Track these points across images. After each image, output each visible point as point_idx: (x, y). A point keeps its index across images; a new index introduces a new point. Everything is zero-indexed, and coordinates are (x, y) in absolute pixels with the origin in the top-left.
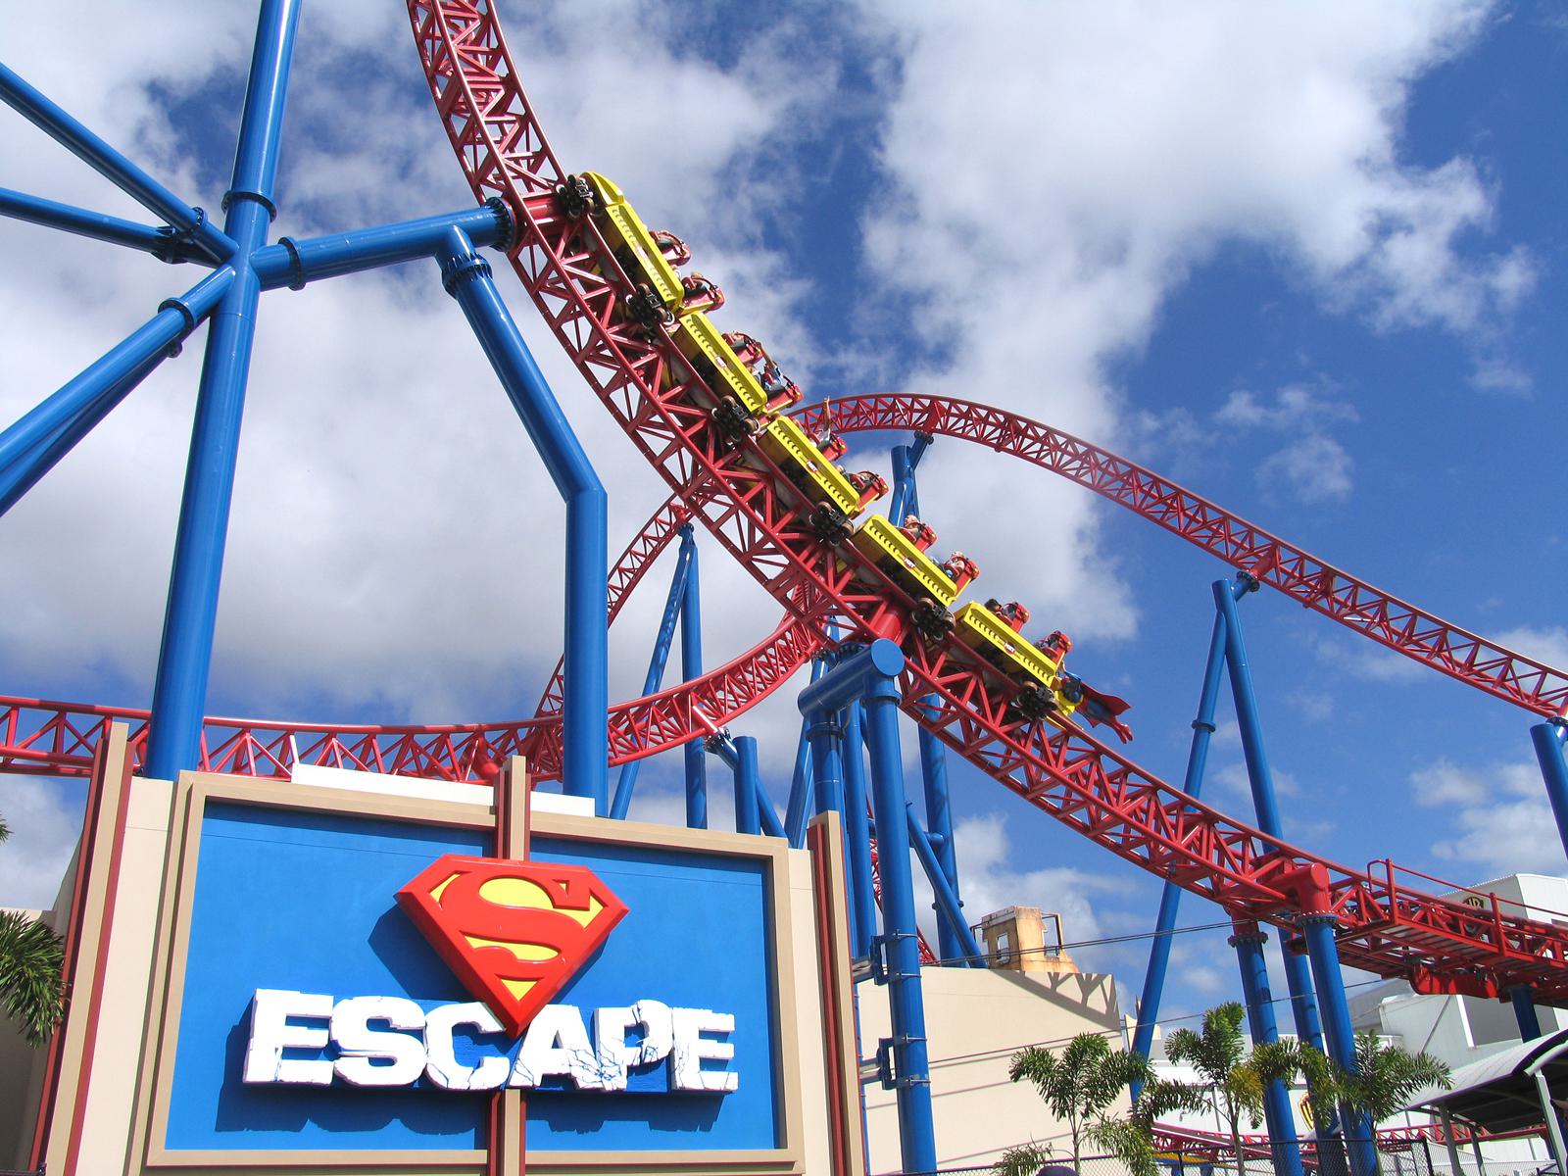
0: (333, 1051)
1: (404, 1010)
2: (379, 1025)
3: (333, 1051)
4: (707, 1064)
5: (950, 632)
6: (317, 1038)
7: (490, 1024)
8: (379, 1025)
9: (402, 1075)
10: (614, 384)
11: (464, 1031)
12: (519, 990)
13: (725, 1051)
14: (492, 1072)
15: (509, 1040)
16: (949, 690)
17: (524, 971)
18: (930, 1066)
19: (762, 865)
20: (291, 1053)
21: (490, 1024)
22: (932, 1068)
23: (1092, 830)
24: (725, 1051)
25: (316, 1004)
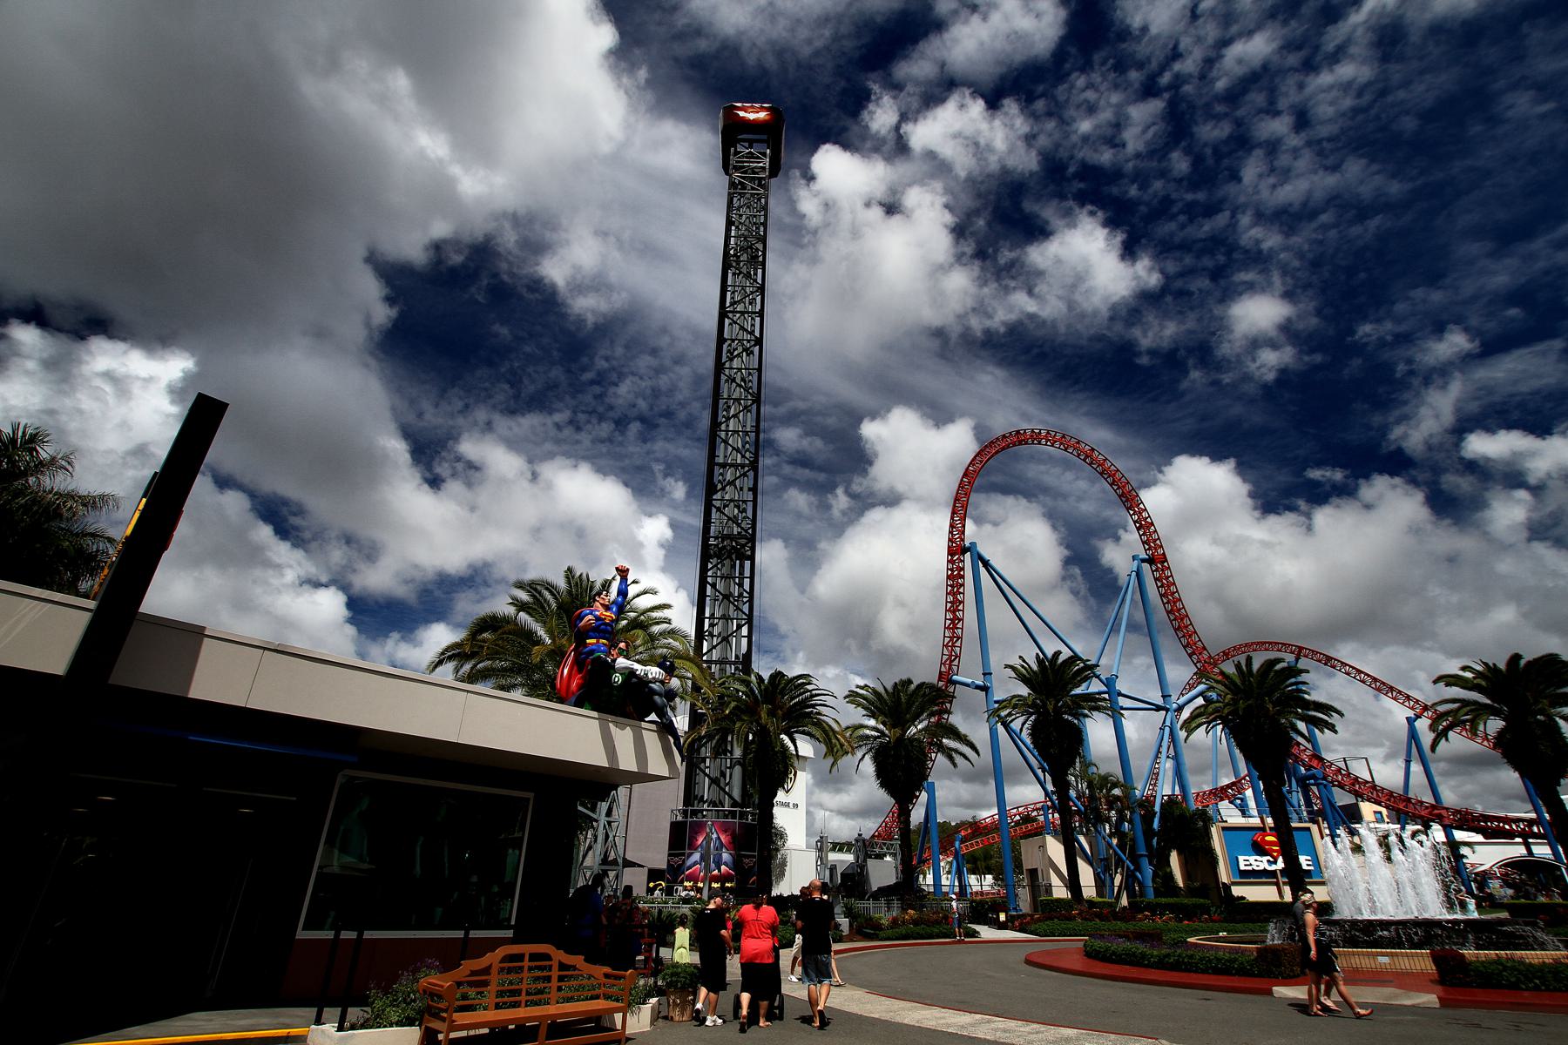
0: (1251, 865)
1: (1258, 858)
2: (1256, 860)
3: (1251, 865)
4: (1308, 865)
5: (1082, 839)
6: (1248, 863)
7: (1272, 860)
8: (1256, 860)
9: (1261, 868)
10: (960, 593)
11: (1268, 861)
12: (1275, 854)
13: (1310, 863)
14: (1273, 867)
15: (1275, 862)
16: (723, 932)
17: (1275, 851)
18: (92, 604)
19: (1308, 829)
20: (1246, 865)
21: (1272, 860)
22: (837, 952)
23: (762, 289)
24: (1310, 863)
25: (1247, 858)
